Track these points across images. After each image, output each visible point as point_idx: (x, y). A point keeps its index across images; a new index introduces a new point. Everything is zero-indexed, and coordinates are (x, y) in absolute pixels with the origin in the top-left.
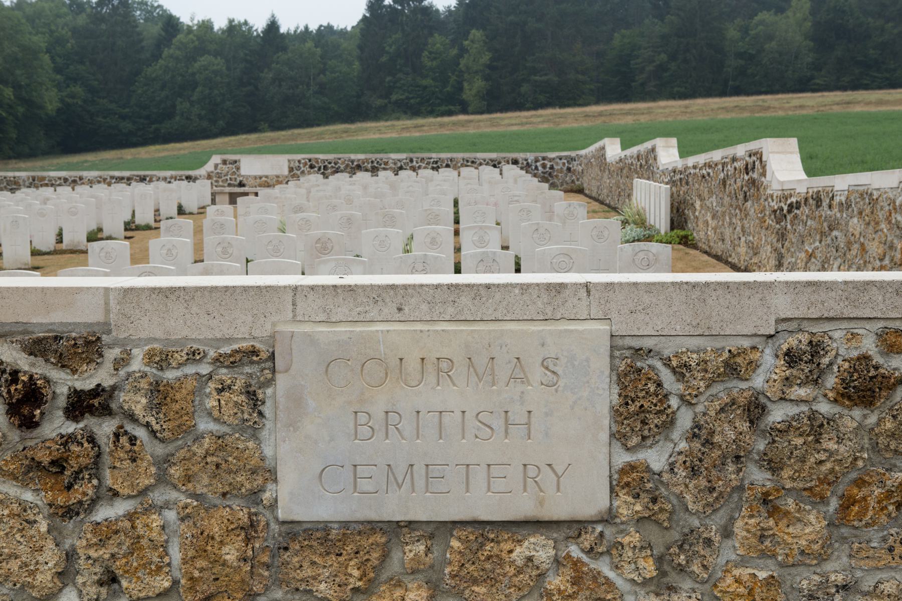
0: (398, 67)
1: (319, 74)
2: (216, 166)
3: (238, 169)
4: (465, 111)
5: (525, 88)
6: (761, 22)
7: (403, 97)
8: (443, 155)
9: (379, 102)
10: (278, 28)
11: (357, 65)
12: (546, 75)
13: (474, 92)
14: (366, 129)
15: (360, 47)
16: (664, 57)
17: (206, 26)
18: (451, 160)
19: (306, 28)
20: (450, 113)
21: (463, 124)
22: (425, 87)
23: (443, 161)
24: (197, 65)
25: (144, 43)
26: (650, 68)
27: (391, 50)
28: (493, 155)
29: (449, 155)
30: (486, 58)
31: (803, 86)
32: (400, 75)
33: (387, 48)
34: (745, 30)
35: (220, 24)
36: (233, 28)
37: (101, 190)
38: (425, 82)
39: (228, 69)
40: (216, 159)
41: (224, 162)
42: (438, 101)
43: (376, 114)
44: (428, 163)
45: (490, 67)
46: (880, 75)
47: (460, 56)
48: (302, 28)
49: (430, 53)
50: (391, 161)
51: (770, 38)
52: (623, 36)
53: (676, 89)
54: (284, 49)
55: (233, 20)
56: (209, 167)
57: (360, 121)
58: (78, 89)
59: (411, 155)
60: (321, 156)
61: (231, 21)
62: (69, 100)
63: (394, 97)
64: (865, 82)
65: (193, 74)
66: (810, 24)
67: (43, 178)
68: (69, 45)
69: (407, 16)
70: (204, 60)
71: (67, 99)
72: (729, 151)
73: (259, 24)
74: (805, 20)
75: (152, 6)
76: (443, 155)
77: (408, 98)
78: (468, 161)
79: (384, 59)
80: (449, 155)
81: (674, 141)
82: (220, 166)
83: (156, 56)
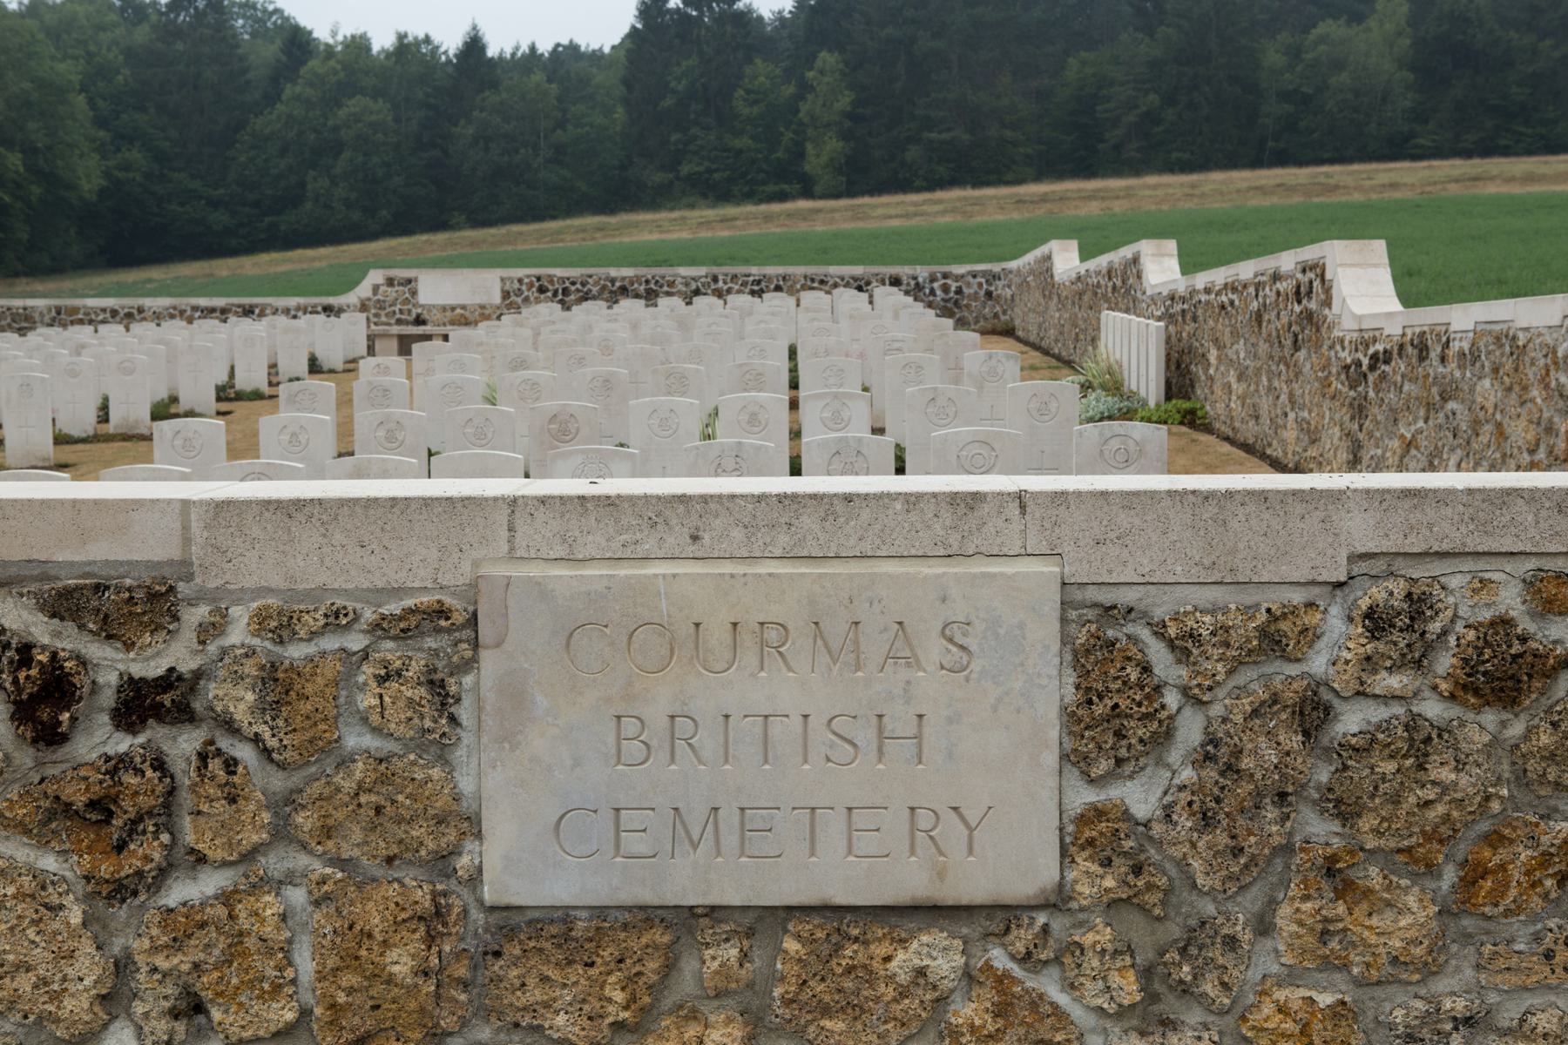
0: (692, 116)
1: (554, 130)
2: (376, 288)
3: (414, 293)
4: (808, 193)
5: (913, 153)
6: (1323, 39)
7: (701, 169)
8: (771, 270)
9: (659, 177)
10: (483, 49)
11: (620, 113)
12: (949, 130)
13: (824, 159)
14: (636, 225)
15: (626, 82)
16: (1154, 98)
17: (358, 45)
18: (784, 279)
19: (533, 48)
20: (782, 197)
21: (805, 216)
22: (739, 152)
23: (770, 280)
24: (342, 113)
25: (251, 76)
26: (1131, 118)
27: (680, 88)
28: (858, 270)
29: (780, 270)
30: (845, 101)
31: (1397, 148)
32: (695, 131)
33: (673, 84)
34: (1295, 53)
35: (382, 41)
36: (405, 49)
37: (176, 331)
38: (738, 143)
39: (397, 120)
40: (376, 276)
41: (390, 282)
42: (761, 176)
43: (655, 198)
44: (744, 284)
45: (852, 116)
46: (1529, 131)
47: (799, 98)
48: (524, 48)
49: (748, 92)
50: (679, 280)
51: (1339, 65)
52: (1084, 63)
53: (1175, 155)
54: (494, 85)
55: (406, 35)
56: (364, 290)
57: (626, 211)
58: (135, 155)
59: (715, 270)
60: (559, 272)
61: (401, 37)
62: (121, 175)
63: (685, 169)
64: (1504, 142)
65: (336, 129)
66: (1408, 42)
67: (75, 310)
68: (120, 78)
69: (708, 29)
70: (355, 104)
71: (116, 173)
72: (1268, 263)
73: (450, 42)
74: (1400, 34)
75: (265, 10)
76: (771, 270)
77: (709, 171)
78: (813, 280)
79: (667, 102)
80: (780, 270)
81: (1171, 245)
82: (382, 289)
83: (272, 98)
